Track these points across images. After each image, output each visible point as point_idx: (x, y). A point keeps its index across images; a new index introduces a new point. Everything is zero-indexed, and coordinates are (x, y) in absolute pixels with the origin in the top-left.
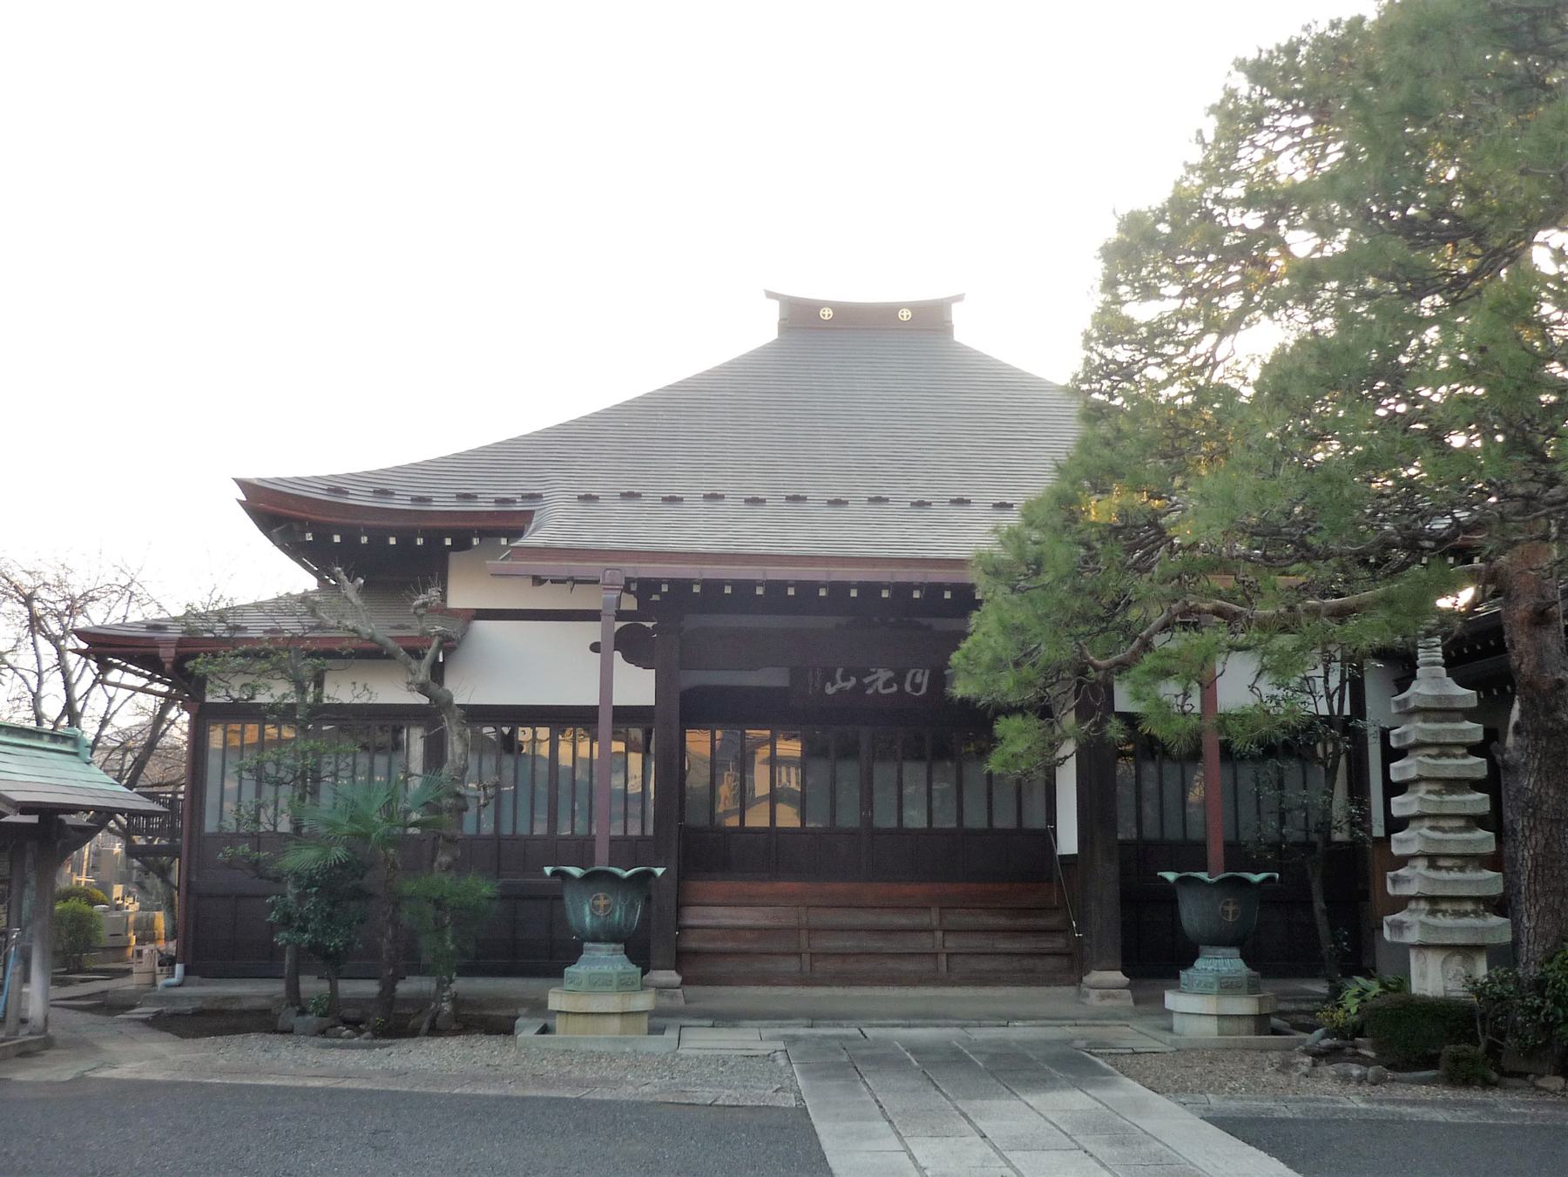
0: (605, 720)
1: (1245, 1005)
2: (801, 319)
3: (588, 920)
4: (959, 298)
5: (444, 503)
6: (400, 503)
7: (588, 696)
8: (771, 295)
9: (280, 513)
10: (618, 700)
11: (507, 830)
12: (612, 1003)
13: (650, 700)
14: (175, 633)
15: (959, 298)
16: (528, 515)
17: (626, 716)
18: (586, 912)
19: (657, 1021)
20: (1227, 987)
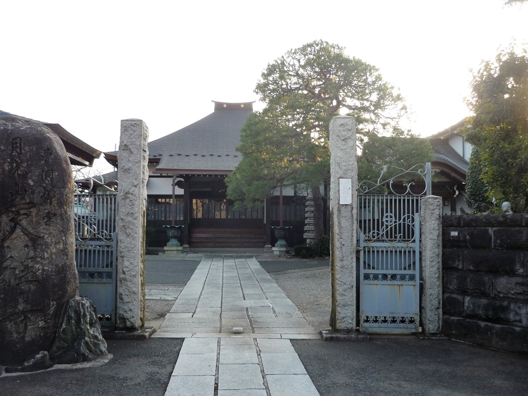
0: (173, 197)
1: (284, 249)
2: (219, 106)
3: (199, 235)
4: (255, 102)
7: (171, 193)
8: (213, 101)
10: (176, 194)
11: (156, 219)
12: (175, 248)
13: (183, 194)
15: (255, 102)
16: (160, 159)
17: (177, 196)
18: (170, 233)
19: (183, 252)
20: (281, 246)
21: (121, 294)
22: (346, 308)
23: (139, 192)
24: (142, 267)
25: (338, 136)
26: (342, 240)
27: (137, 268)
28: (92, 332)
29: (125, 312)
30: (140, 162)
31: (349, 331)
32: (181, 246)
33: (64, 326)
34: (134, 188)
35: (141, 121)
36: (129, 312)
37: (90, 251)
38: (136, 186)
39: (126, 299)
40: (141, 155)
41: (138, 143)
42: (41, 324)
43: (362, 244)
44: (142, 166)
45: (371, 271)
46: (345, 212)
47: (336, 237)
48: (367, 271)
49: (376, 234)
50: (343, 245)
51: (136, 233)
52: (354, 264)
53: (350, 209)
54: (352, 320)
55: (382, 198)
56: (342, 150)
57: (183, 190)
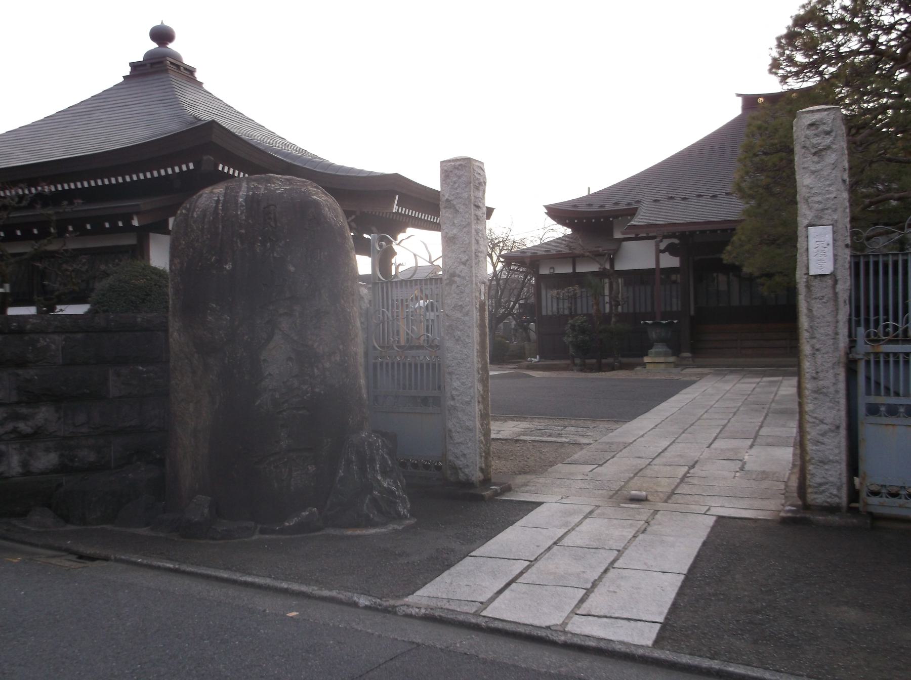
5: (610, 207)
6: (595, 208)
8: (739, 95)
9: (557, 213)
12: (662, 360)
14: (529, 254)
16: (636, 209)
18: (653, 334)
19: (676, 366)
21: (450, 431)
22: (826, 467)
23: (471, 272)
24: (481, 388)
25: (804, 147)
26: (815, 341)
27: (472, 390)
28: (385, 485)
29: (457, 458)
30: (469, 224)
31: (832, 509)
32: (673, 355)
33: (341, 473)
34: (462, 266)
35: (469, 160)
36: (462, 459)
37: (398, 364)
38: (464, 264)
39: (457, 438)
40: (470, 214)
41: (465, 195)
42: (312, 469)
43: (863, 347)
44: (473, 231)
45: (883, 400)
46: (822, 290)
47: (804, 335)
48: (873, 399)
49: (890, 329)
50: (818, 350)
51: (468, 336)
52: (842, 386)
53: (830, 282)
54: (839, 489)
55: (885, 259)
56: (813, 172)
57: (678, 258)
